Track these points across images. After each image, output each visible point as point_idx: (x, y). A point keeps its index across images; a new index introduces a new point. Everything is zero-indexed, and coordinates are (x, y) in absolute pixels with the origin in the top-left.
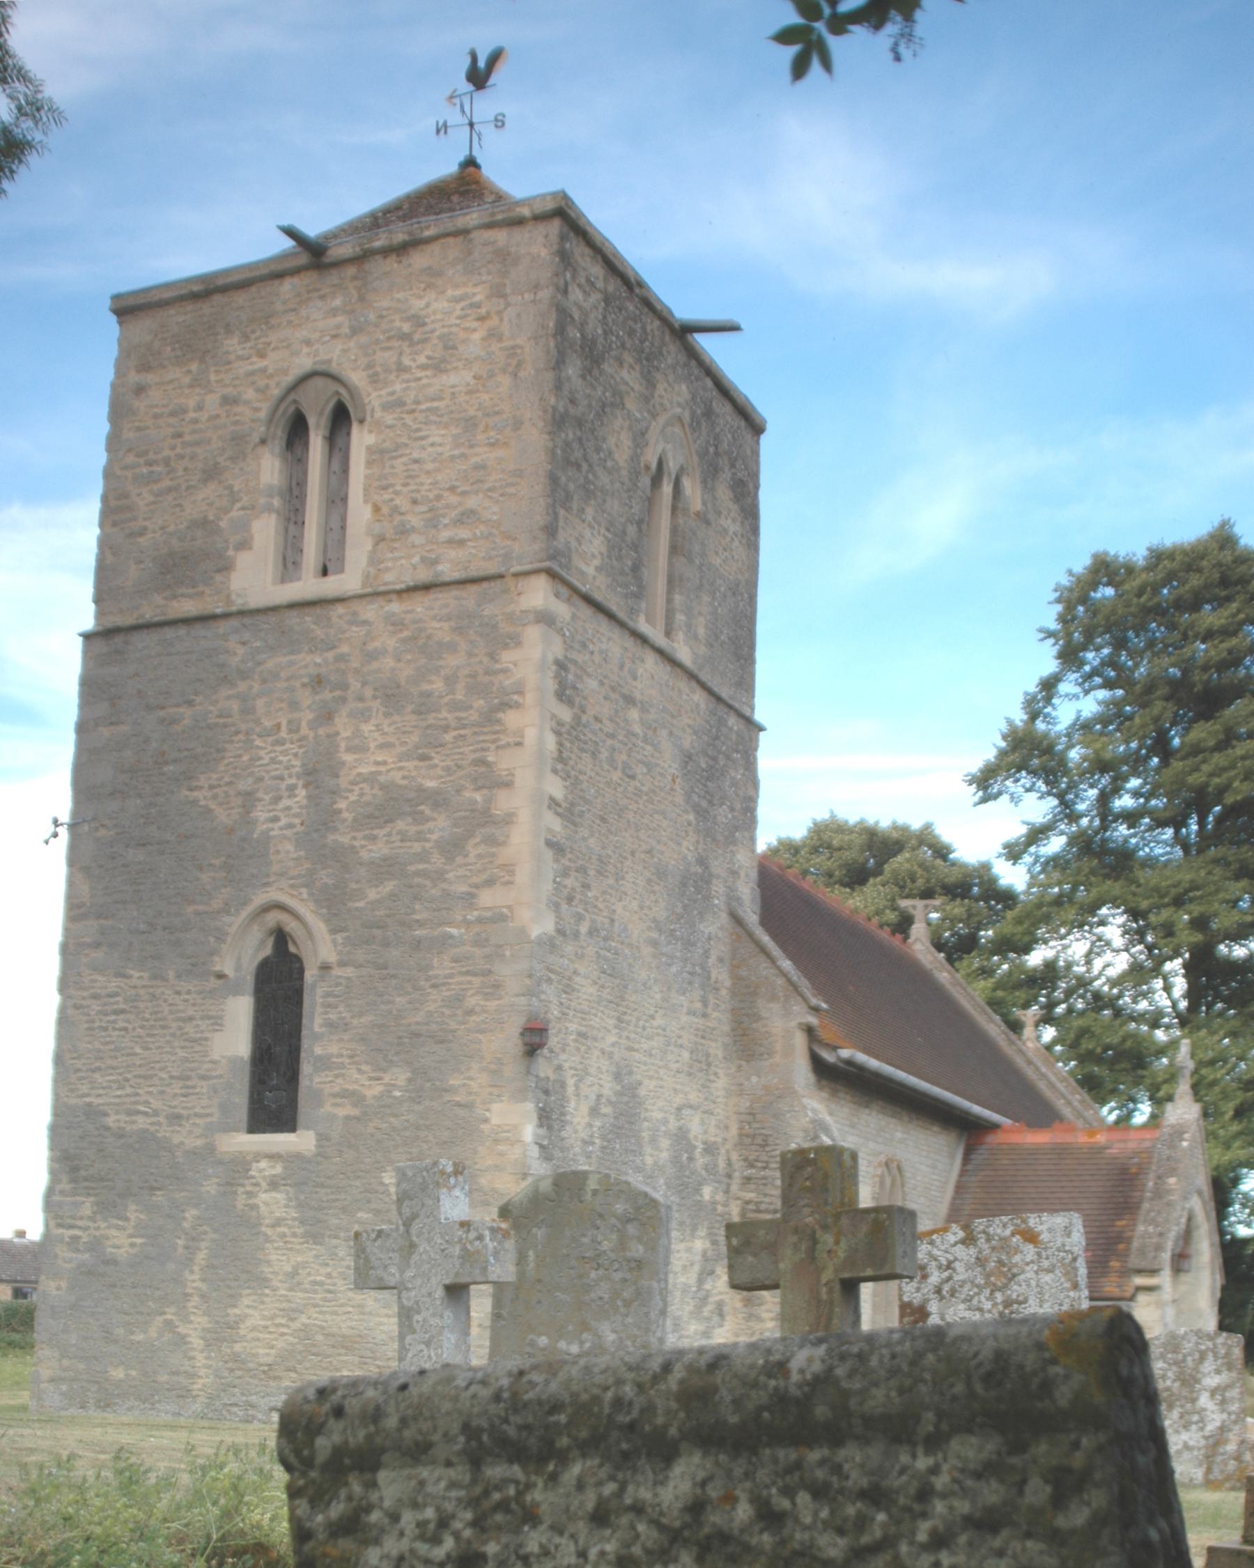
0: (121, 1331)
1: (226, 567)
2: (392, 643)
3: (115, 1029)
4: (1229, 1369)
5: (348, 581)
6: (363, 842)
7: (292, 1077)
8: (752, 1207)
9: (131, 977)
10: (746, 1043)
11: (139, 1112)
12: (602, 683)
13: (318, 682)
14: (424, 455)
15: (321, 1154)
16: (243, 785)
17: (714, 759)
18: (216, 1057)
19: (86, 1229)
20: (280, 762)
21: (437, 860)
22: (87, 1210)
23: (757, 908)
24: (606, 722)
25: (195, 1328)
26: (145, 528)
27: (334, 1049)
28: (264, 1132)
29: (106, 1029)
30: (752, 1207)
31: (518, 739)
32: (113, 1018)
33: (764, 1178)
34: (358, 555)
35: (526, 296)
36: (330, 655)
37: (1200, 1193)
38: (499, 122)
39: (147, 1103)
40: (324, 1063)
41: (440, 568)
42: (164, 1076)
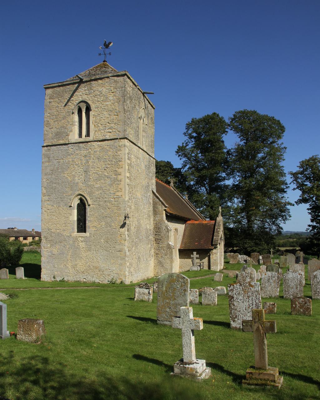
2: (98, 149)
3: (52, 215)
4: (251, 278)
5: (91, 138)
7: (85, 224)
8: (157, 239)
10: (155, 212)
12: (134, 156)
16: (73, 173)
17: (149, 166)
18: (71, 220)
19: (49, 249)
20: (79, 170)
22: (49, 246)
23: (155, 189)
24: (135, 163)
25: (69, 265)
26: (52, 127)
28: (80, 233)
30: (157, 239)
33: (159, 234)
34: (91, 134)
35: (120, 89)
36: (87, 151)
38: (110, 54)
39: (59, 228)
41: (107, 136)
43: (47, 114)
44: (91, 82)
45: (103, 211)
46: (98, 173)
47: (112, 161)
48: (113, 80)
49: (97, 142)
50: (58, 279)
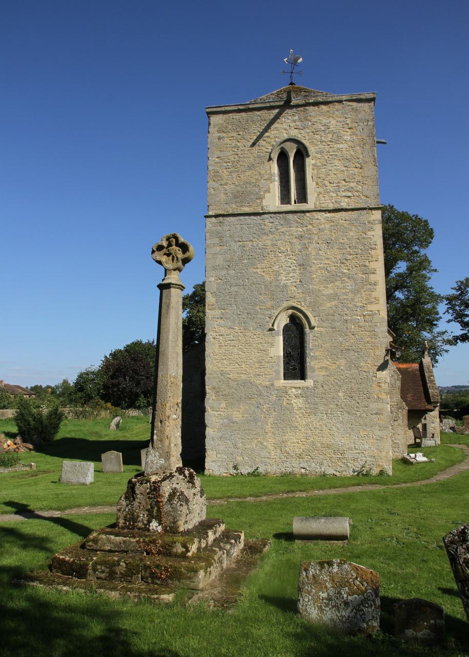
0: (240, 444)
1: (261, 198)
5: (310, 205)
6: (324, 289)
9: (235, 329)
11: (242, 373)
13: (301, 237)
14: (333, 168)
15: (315, 387)
16: (276, 268)
18: (272, 356)
21: (351, 296)
22: (223, 405)
25: (269, 443)
27: (317, 354)
29: (227, 346)
31: (377, 259)
32: (230, 342)
37: (312, 328)
40: (315, 358)
42: (251, 361)
43: (213, 159)
44: (307, 108)
45: (341, 339)
46: (328, 269)
47: (356, 248)
48: (350, 107)
49: (323, 213)
50: (245, 470)
